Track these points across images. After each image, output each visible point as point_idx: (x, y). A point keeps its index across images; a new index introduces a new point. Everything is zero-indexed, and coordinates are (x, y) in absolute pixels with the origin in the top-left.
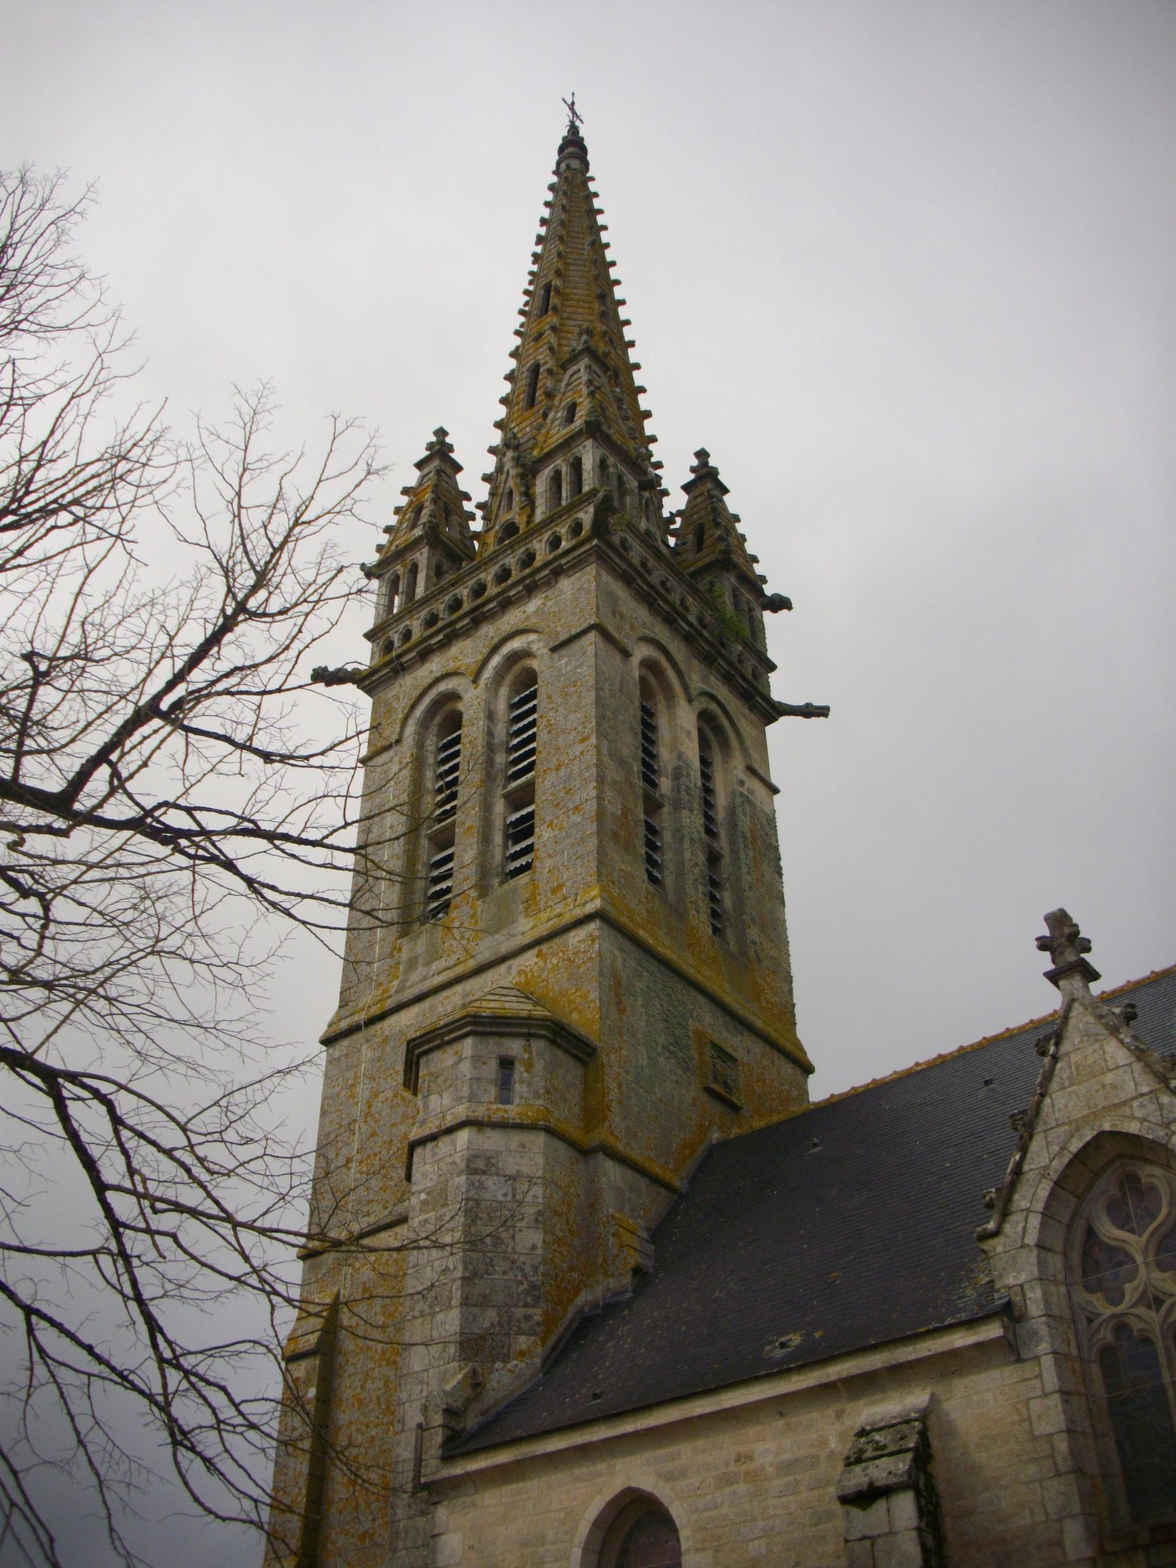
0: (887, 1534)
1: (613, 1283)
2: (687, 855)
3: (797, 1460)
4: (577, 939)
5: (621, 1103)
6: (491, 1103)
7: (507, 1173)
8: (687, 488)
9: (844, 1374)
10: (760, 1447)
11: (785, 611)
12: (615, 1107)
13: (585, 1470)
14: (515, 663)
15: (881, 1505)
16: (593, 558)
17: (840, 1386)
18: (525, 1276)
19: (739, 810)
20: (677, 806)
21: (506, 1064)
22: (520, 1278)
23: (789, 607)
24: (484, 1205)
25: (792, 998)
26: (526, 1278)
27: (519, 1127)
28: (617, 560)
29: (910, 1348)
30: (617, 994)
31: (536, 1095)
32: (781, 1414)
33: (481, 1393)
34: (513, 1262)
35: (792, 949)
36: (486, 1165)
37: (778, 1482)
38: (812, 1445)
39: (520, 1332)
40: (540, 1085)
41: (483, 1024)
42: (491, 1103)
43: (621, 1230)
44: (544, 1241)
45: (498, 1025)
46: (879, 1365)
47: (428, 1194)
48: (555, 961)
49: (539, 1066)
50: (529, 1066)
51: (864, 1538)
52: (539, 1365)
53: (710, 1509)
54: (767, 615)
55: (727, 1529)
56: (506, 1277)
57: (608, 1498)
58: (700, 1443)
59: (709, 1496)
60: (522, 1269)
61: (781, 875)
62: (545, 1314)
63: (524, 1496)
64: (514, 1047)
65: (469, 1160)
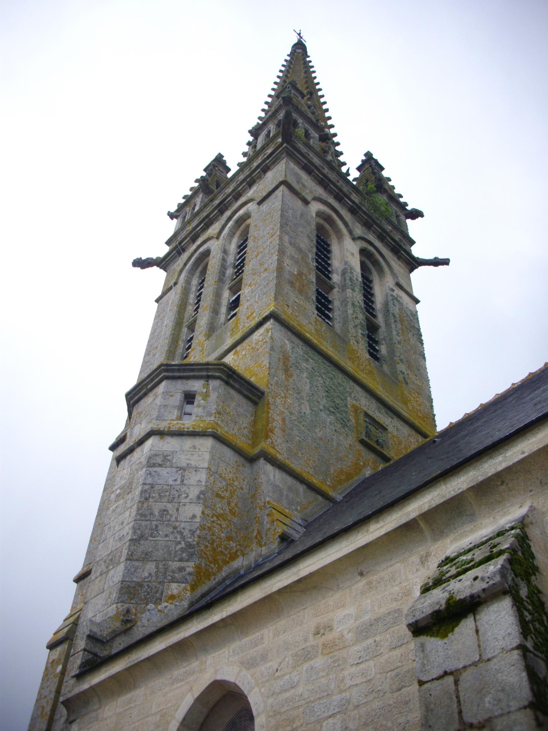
0: (475, 664)
1: (264, 550)
2: (350, 311)
3: (377, 620)
4: (259, 334)
5: (284, 431)
6: (173, 420)
7: (179, 465)
8: (359, 169)
9: (426, 508)
10: (340, 614)
11: (419, 218)
12: (277, 431)
13: (182, 670)
14: (242, 224)
15: (467, 625)
16: (284, 155)
17: (422, 524)
18: (183, 538)
19: (391, 303)
20: (343, 288)
21: (189, 398)
22: (179, 539)
23: (422, 216)
24: (157, 488)
25: (433, 411)
26: (184, 540)
27: (193, 434)
28: (300, 157)
29: (500, 458)
30: (286, 365)
31: (209, 414)
32: (361, 574)
33: (130, 628)
34: (175, 528)
35: (431, 384)
36: (163, 461)
37: (356, 648)
38: (396, 600)
39: (173, 580)
40: (213, 408)
41: (173, 371)
42: (173, 420)
43: (273, 510)
44: (203, 513)
45: (184, 370)
46: (465, 487)
47: (121, 489)
48: (243, 353)
49: (213, 396)
50: (206, 396)
51: (446, 673)
52: (186, 606)
53: (287, 690)
54: (409, 221)
55: (301, 709)
56: (167, 539)
57: (196, 695)
58: (282, 623)
59: (287, 677)
60: (181, 533)
61: (422, 344)
62: (198, 567)
63: (132, 705)
64: (196, 386)
65: (150, 458)
